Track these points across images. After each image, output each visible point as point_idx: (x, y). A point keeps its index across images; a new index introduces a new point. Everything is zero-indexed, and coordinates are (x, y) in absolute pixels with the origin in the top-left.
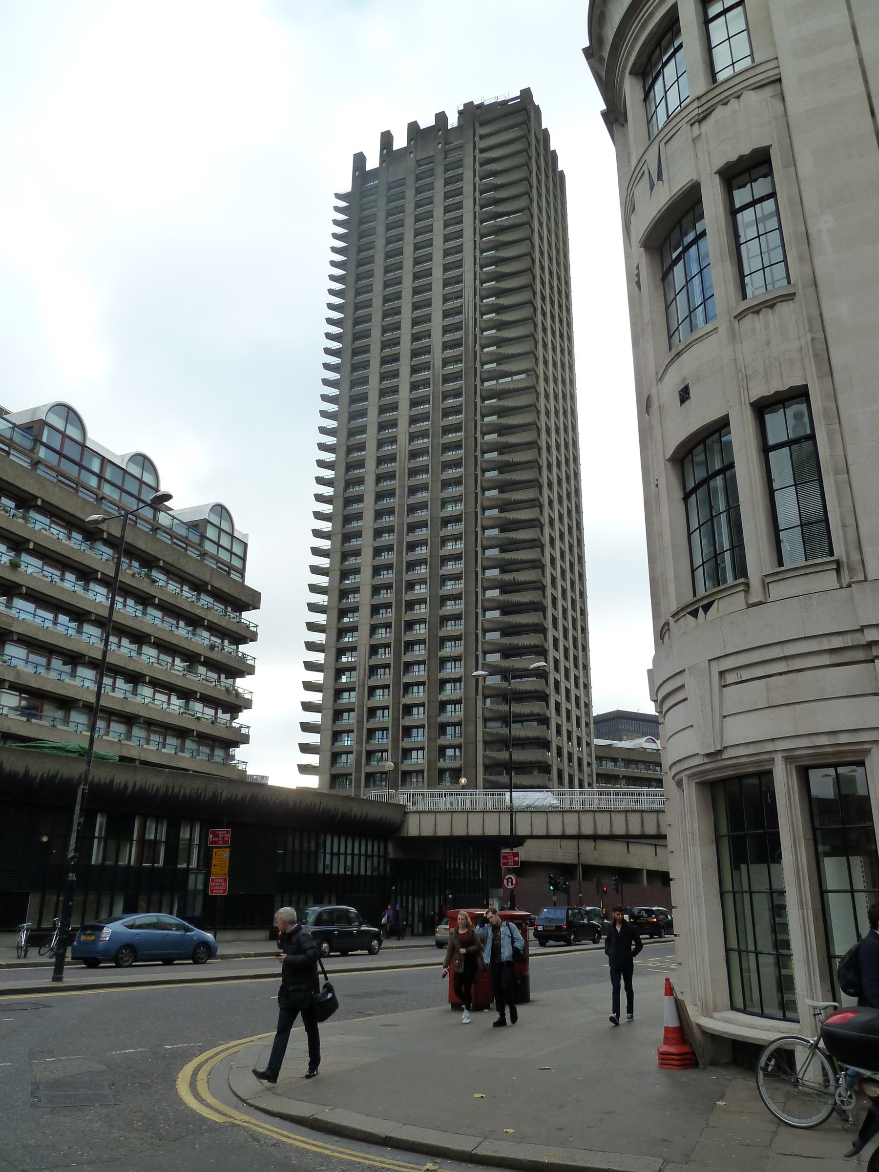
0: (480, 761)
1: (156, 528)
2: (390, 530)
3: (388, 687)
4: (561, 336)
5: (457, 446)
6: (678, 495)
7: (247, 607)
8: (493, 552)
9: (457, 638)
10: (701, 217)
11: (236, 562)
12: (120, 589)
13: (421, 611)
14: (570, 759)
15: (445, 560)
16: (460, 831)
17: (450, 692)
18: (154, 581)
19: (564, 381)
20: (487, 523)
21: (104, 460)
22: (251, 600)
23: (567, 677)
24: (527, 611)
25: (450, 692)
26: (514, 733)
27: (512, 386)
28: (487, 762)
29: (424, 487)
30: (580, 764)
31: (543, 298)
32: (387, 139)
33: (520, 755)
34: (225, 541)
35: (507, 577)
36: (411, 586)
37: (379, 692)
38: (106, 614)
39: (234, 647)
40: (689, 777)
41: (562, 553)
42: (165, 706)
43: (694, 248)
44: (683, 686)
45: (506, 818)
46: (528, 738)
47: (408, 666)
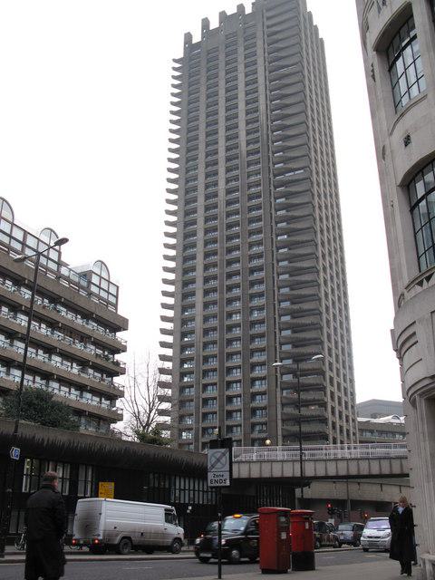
0: (280, 433)
1: (59, 276)
2: (215, 265)
3: (215, 384)
4: (326, 144)
5: (259, 219)
6: (407, 209)
7: (119, 329)
8: (285, 291)
9: (262, 350)
10: (413, 27)
11: (112, 299)
12: (31, 342)
13: (237, 332)
14: (341, 431)
15: (252, 297)
16: (266, 474)
17: (258, 387)
18: (58, 312)
19: (329, 174)
20: (280, 270)
21: (26, 233)
22: (121, 325)
23: (338, 375)
24: (310, 330)
25: (258, 387)
26: (302, 413)
27: (294, 178)
28: (285, 433)
29: (237, 248)
30: (348, 435)
31: (313, 120)
32: (205, 23)
33: (306, 428)
34: (104, 285)
35: (296, 307)
36: (230, 315)
37: (210, 388)
38: (25, 332)
39: (110, 379)
40: (420, 395)
41: (333, 290)
42: (69, 369)
43: (409, 48)
44: (414, 333)
45: (298, 466)
46: (312, 416)
47: (229, 370)
